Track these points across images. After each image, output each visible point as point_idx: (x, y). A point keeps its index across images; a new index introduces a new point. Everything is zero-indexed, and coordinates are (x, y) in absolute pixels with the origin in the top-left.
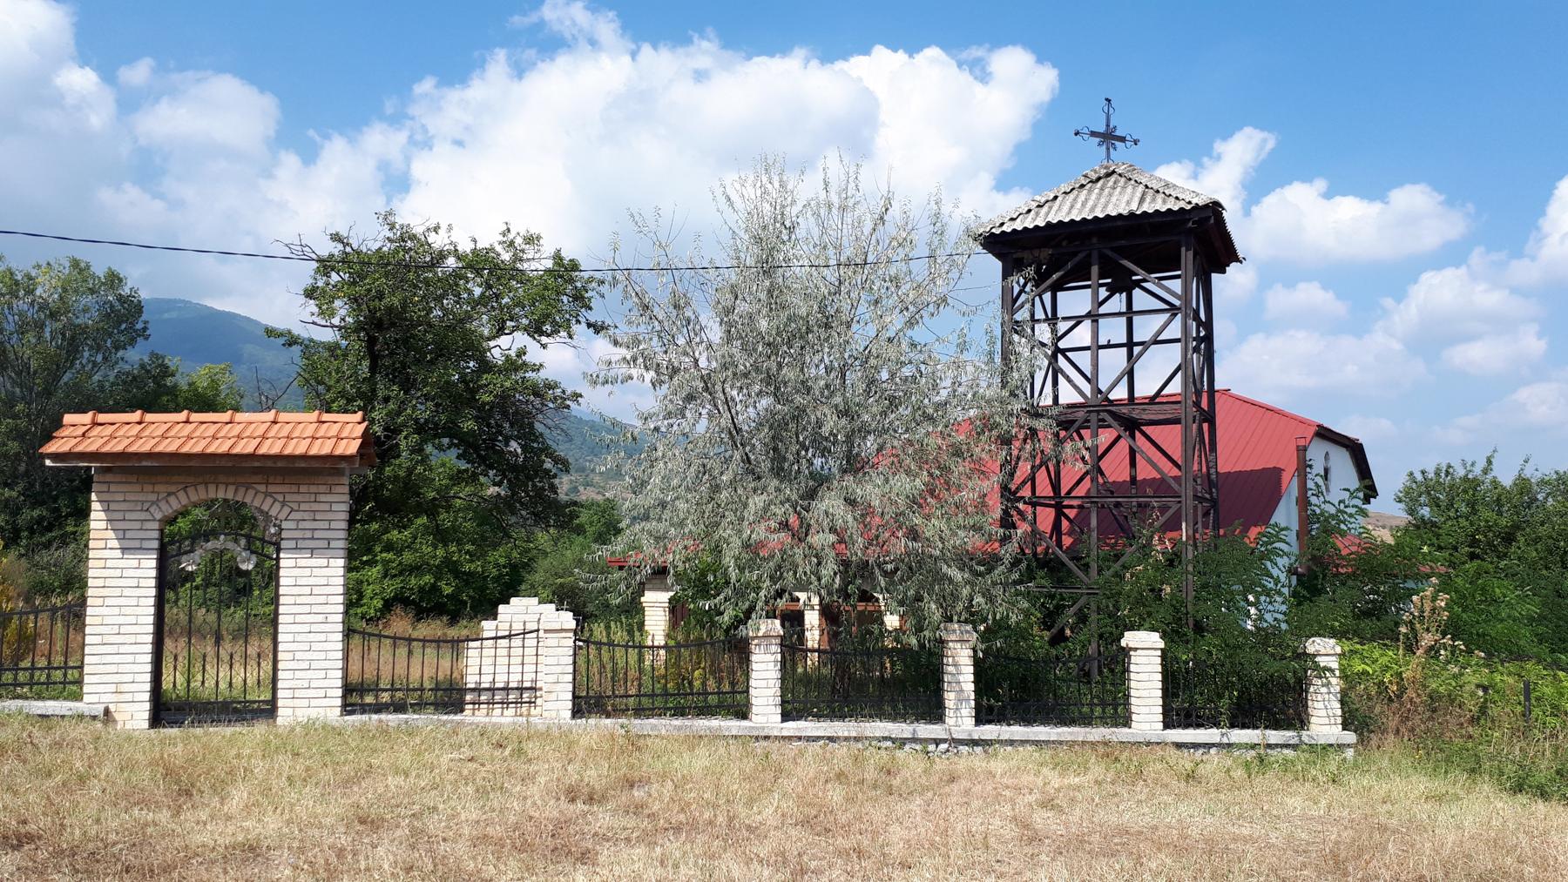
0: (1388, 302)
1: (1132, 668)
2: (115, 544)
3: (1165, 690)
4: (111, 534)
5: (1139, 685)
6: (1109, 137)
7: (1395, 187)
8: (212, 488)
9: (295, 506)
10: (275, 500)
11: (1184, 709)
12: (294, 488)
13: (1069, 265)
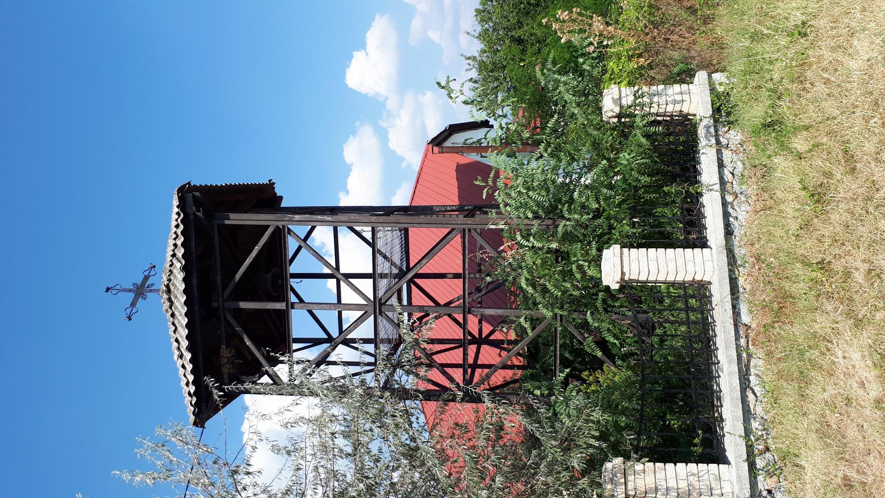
0: (404, 164)
1: (643, 278)
3: (666, 246)
5: (654, 270)
6: (141, 290)
11: (684, 227)
13: (238, 329)
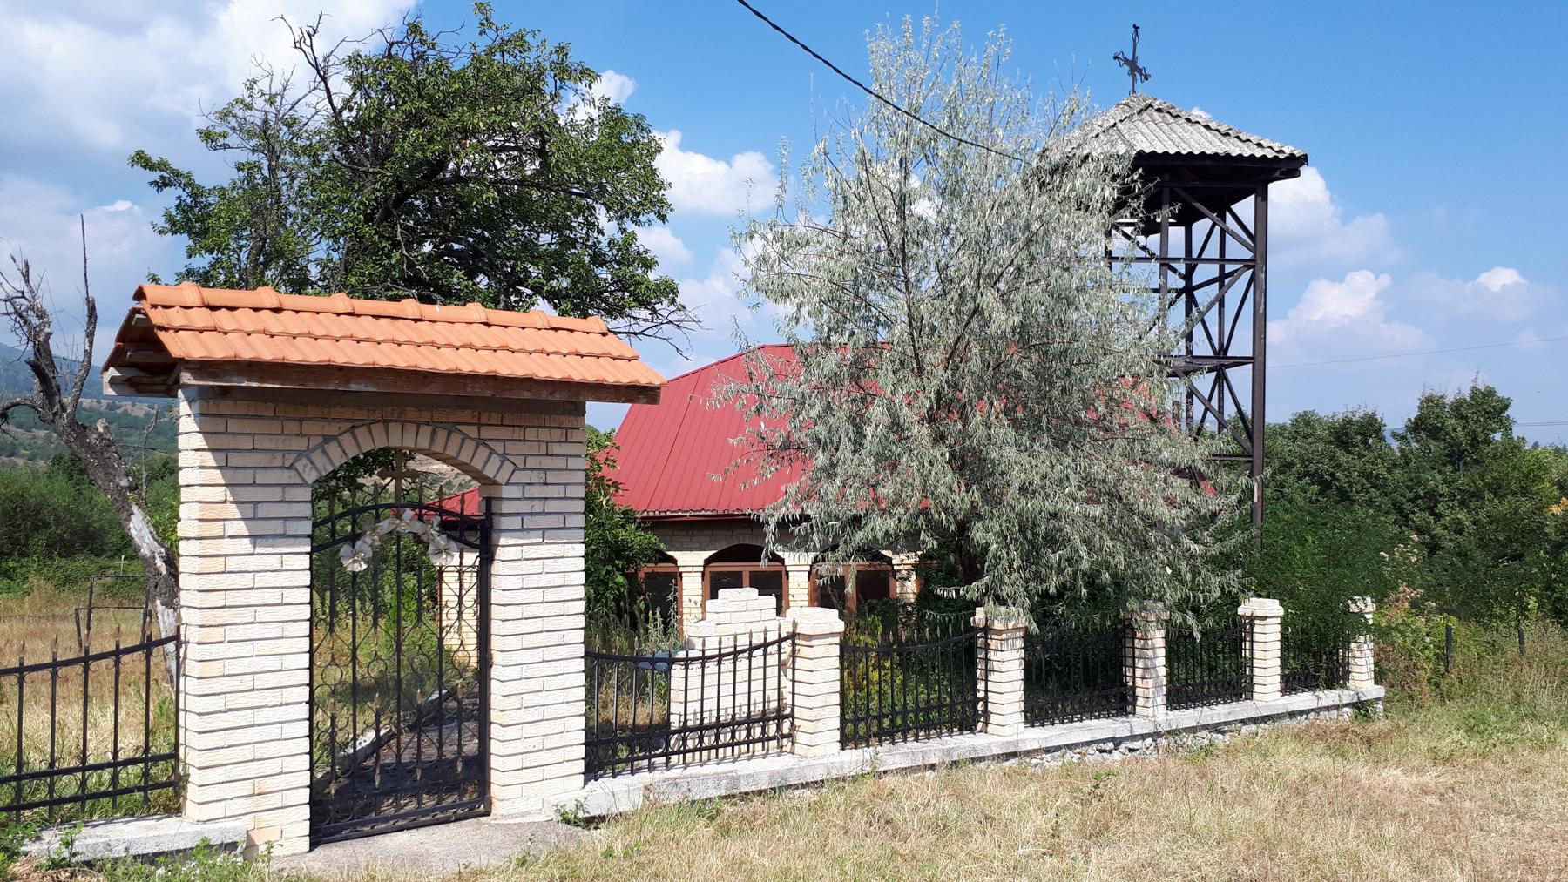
2: (240, 528)
4: (233, 510)
7: (737, 153)
8: (395, 428)
9: (519, 462)
10: (492, 452)
12: (518, 433)
